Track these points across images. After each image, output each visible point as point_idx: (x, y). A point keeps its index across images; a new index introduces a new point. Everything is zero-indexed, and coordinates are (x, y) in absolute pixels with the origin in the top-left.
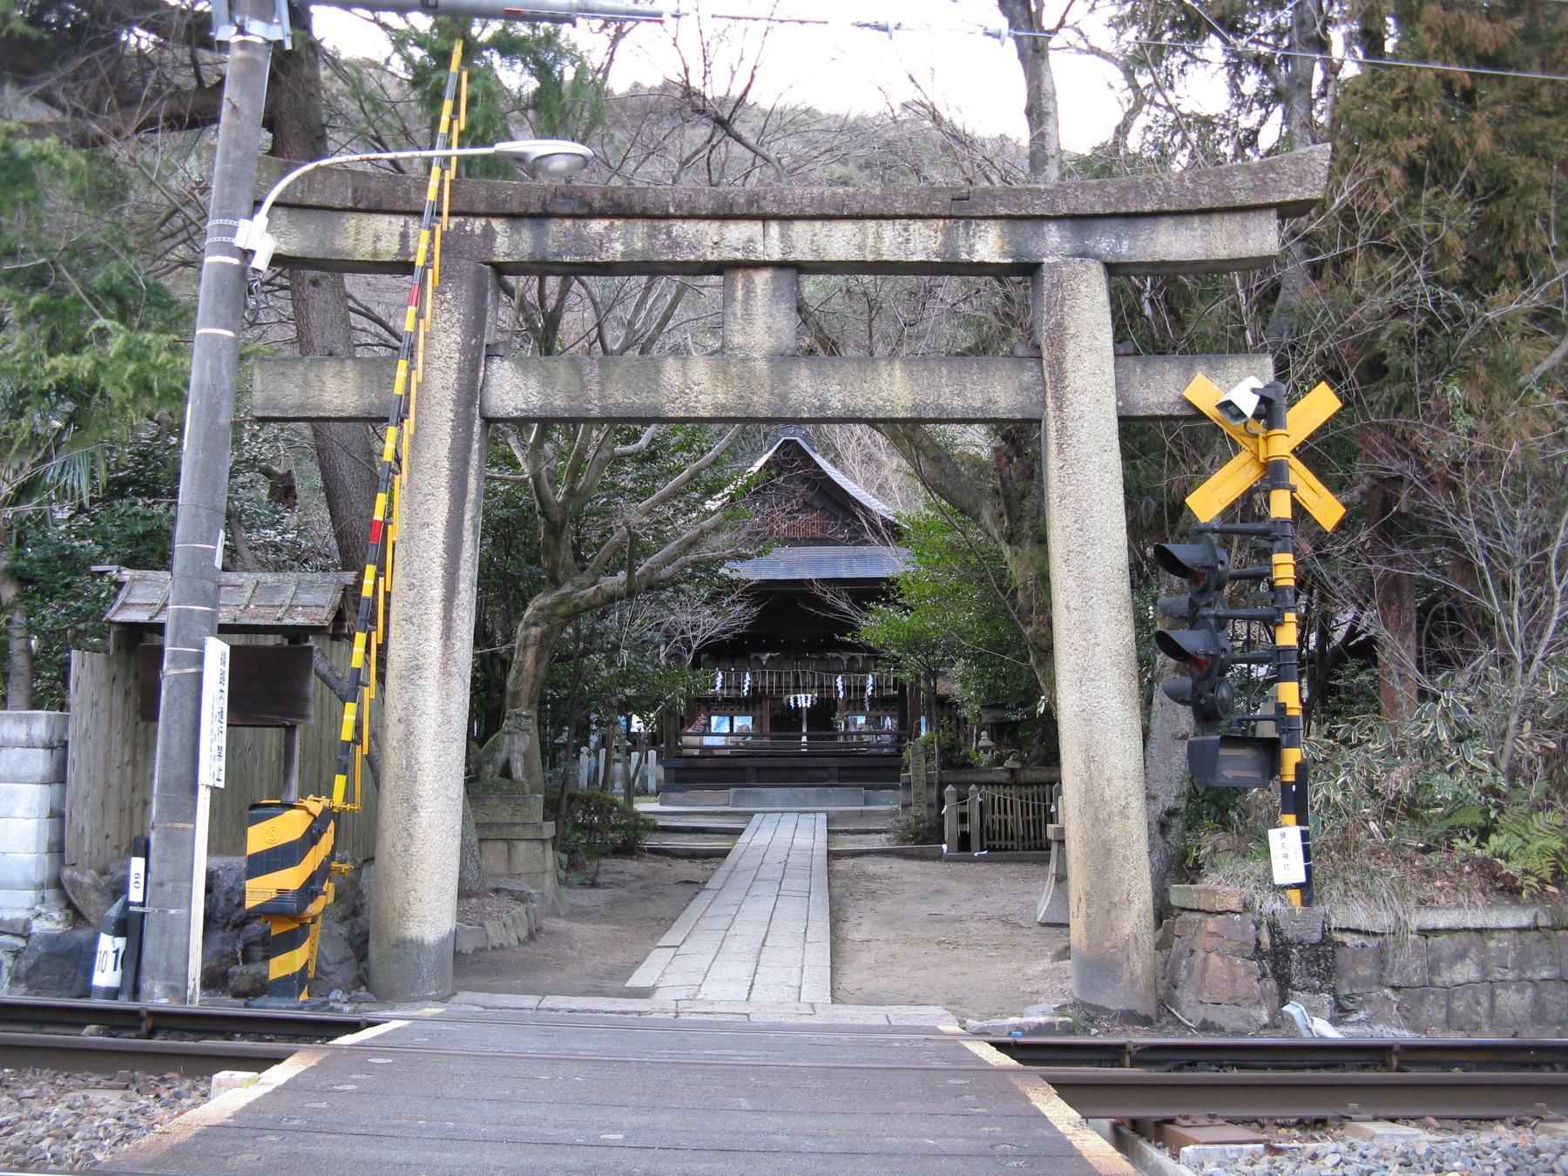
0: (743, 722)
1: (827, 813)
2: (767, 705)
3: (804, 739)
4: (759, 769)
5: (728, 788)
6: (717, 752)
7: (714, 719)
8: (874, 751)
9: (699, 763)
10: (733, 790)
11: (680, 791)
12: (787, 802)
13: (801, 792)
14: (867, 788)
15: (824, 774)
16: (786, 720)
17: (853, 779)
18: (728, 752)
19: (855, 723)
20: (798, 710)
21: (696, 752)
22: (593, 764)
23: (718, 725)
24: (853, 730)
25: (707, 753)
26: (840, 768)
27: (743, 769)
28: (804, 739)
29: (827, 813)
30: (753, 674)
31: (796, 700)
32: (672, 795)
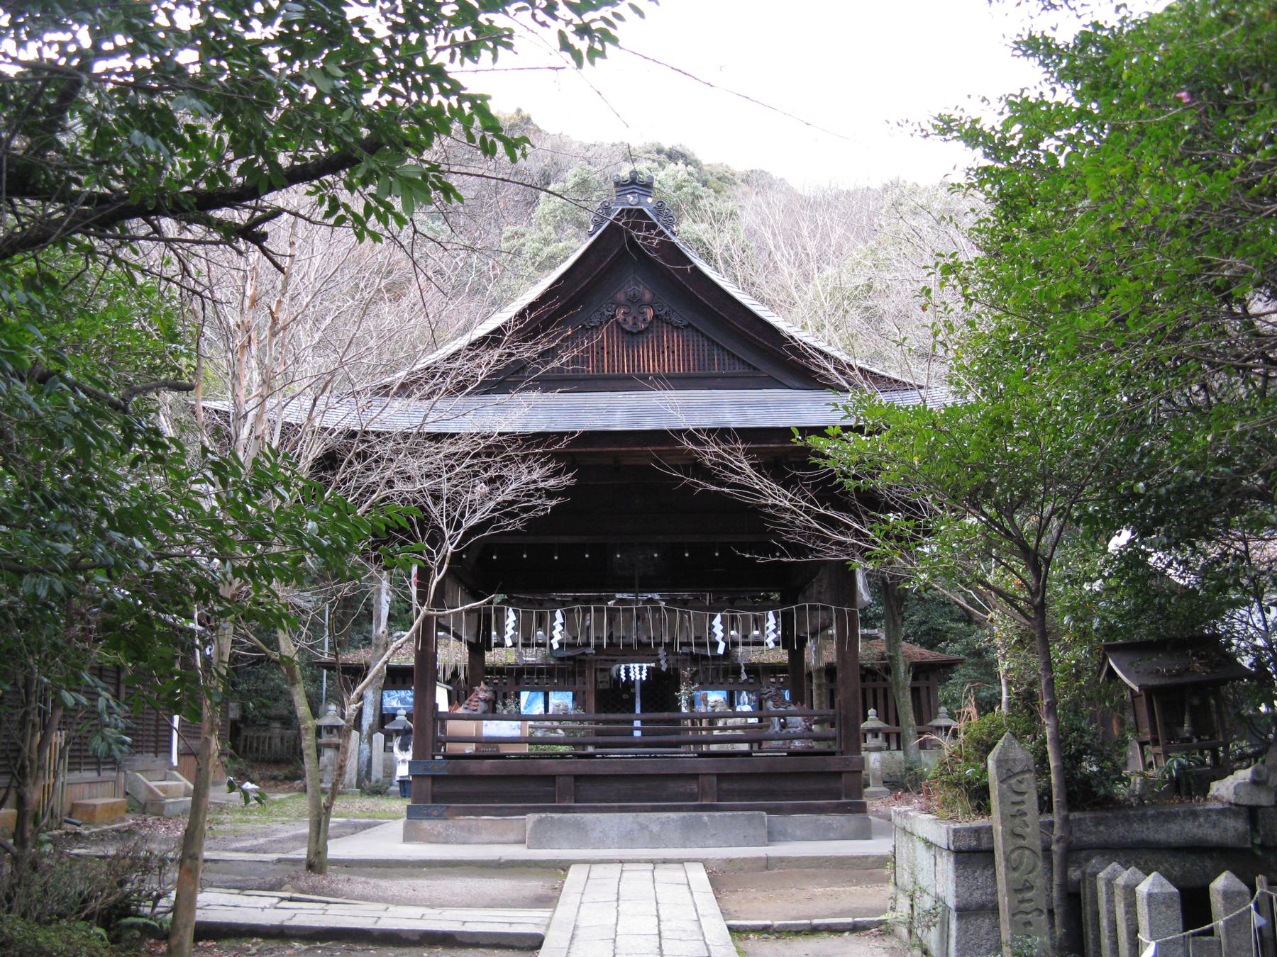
0: (561, 700)
1: (705, 863)
2: (590, 675)
3: (637, 724)
4: (578, 778)
5: (524, 811)
6: (505, 749)
7: (524, 696)
8: (729, 732)
9: (474, 767)
10: (531, 818)
11: (440, 817)
12: (628, 839)
13: (653, 820)
14: (771, 811)
15: (694, 787)
16: (614, 697)
17: (742, 795)
18: (525, 749)
19: (705, 701)
20: (629, 683)
21: (469, 749)
22: (366, 753)
23: (529, 703)
24: (703, 709)
25: (488, 750)
26: (721, 777)
27: (551, 778)
28: (637, 724)
29: (705, 863)
30: (567, 615)
31: (627, 671)
32: (426, 825)
